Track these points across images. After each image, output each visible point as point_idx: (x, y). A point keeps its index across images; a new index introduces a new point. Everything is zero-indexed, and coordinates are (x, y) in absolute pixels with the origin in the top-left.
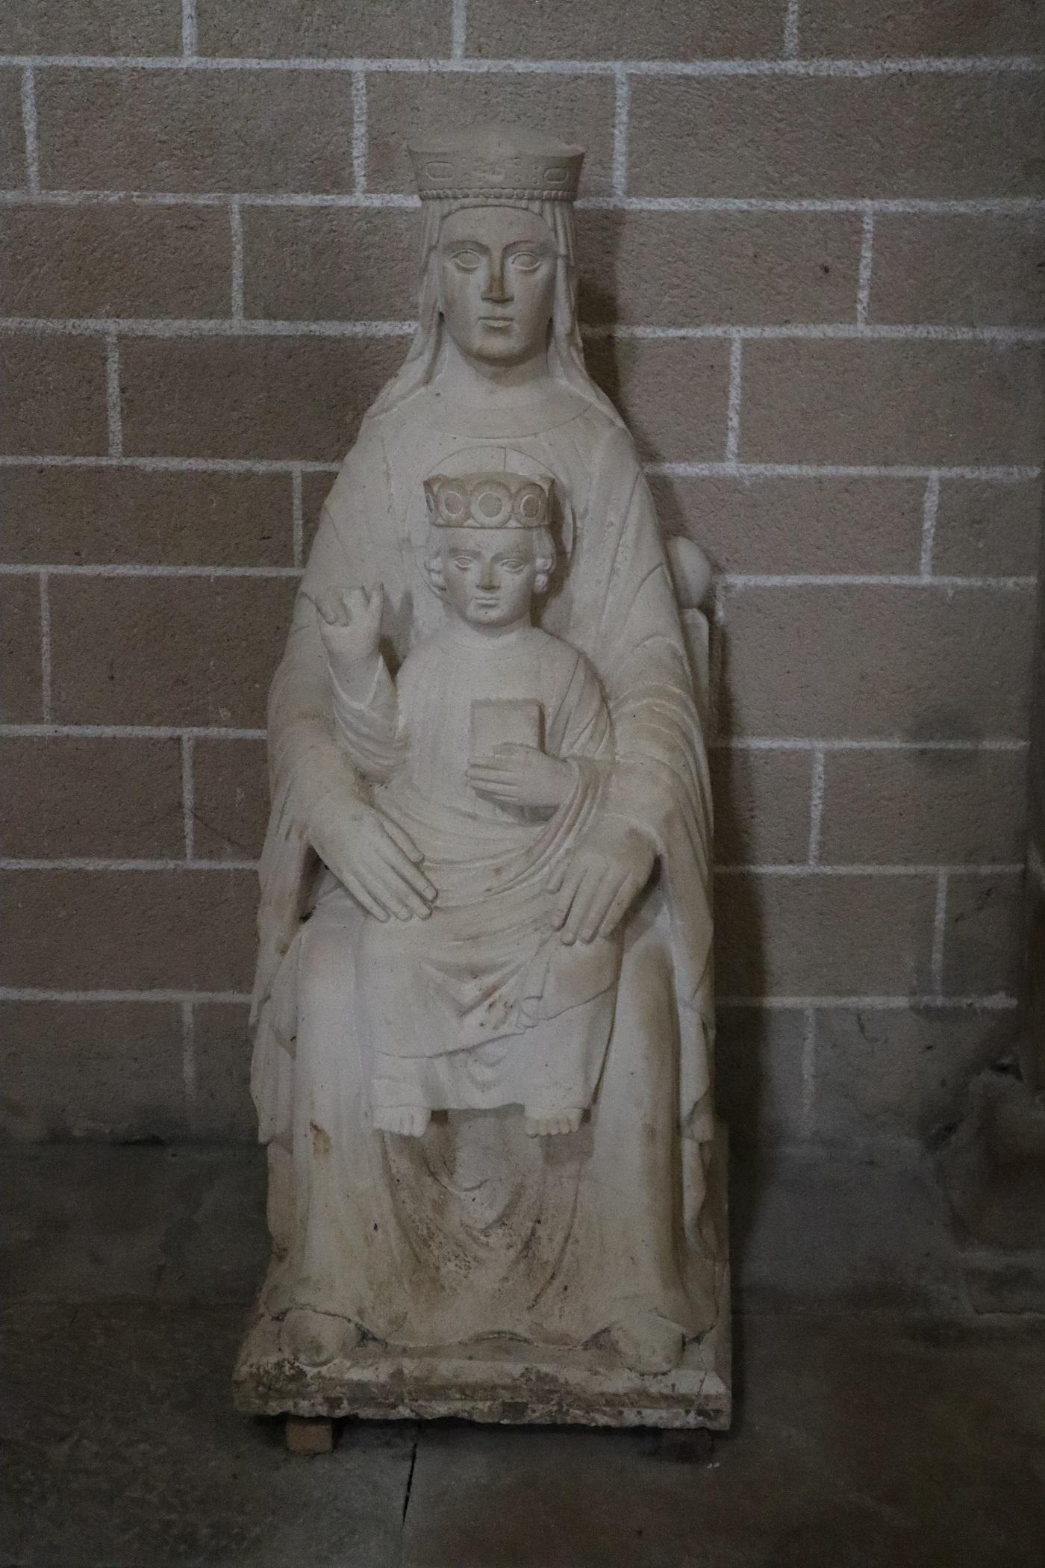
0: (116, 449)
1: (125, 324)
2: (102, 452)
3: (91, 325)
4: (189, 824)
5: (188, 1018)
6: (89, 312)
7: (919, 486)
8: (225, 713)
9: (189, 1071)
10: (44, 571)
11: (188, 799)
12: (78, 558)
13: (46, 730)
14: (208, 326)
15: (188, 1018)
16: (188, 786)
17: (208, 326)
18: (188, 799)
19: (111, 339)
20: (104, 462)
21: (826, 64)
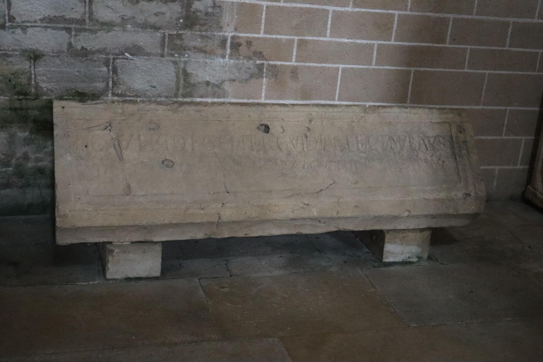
0: (507, 46)
1: (515, 19)
2: (504, 46)
3: (508, 19)
4: (505, 128)
5: (497, 172)
6: (508, 16)
7: (510, 46)
8: (516, 104)
9: (495, 184)
10: (487, 72)
11: (506, 123)
12: (495, 69)
13: (481, 107)
14: (529, 20)
15: (497, 172)
16: (506, 120)
17: (529, 20)
18: (506, 123)
19: (511, 22)
20: (504, 49)
21: (39, 78)
